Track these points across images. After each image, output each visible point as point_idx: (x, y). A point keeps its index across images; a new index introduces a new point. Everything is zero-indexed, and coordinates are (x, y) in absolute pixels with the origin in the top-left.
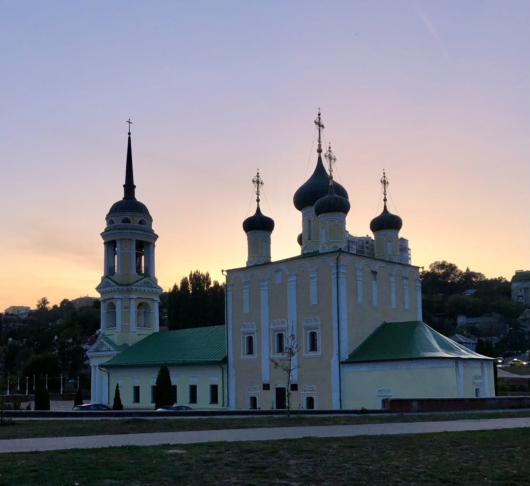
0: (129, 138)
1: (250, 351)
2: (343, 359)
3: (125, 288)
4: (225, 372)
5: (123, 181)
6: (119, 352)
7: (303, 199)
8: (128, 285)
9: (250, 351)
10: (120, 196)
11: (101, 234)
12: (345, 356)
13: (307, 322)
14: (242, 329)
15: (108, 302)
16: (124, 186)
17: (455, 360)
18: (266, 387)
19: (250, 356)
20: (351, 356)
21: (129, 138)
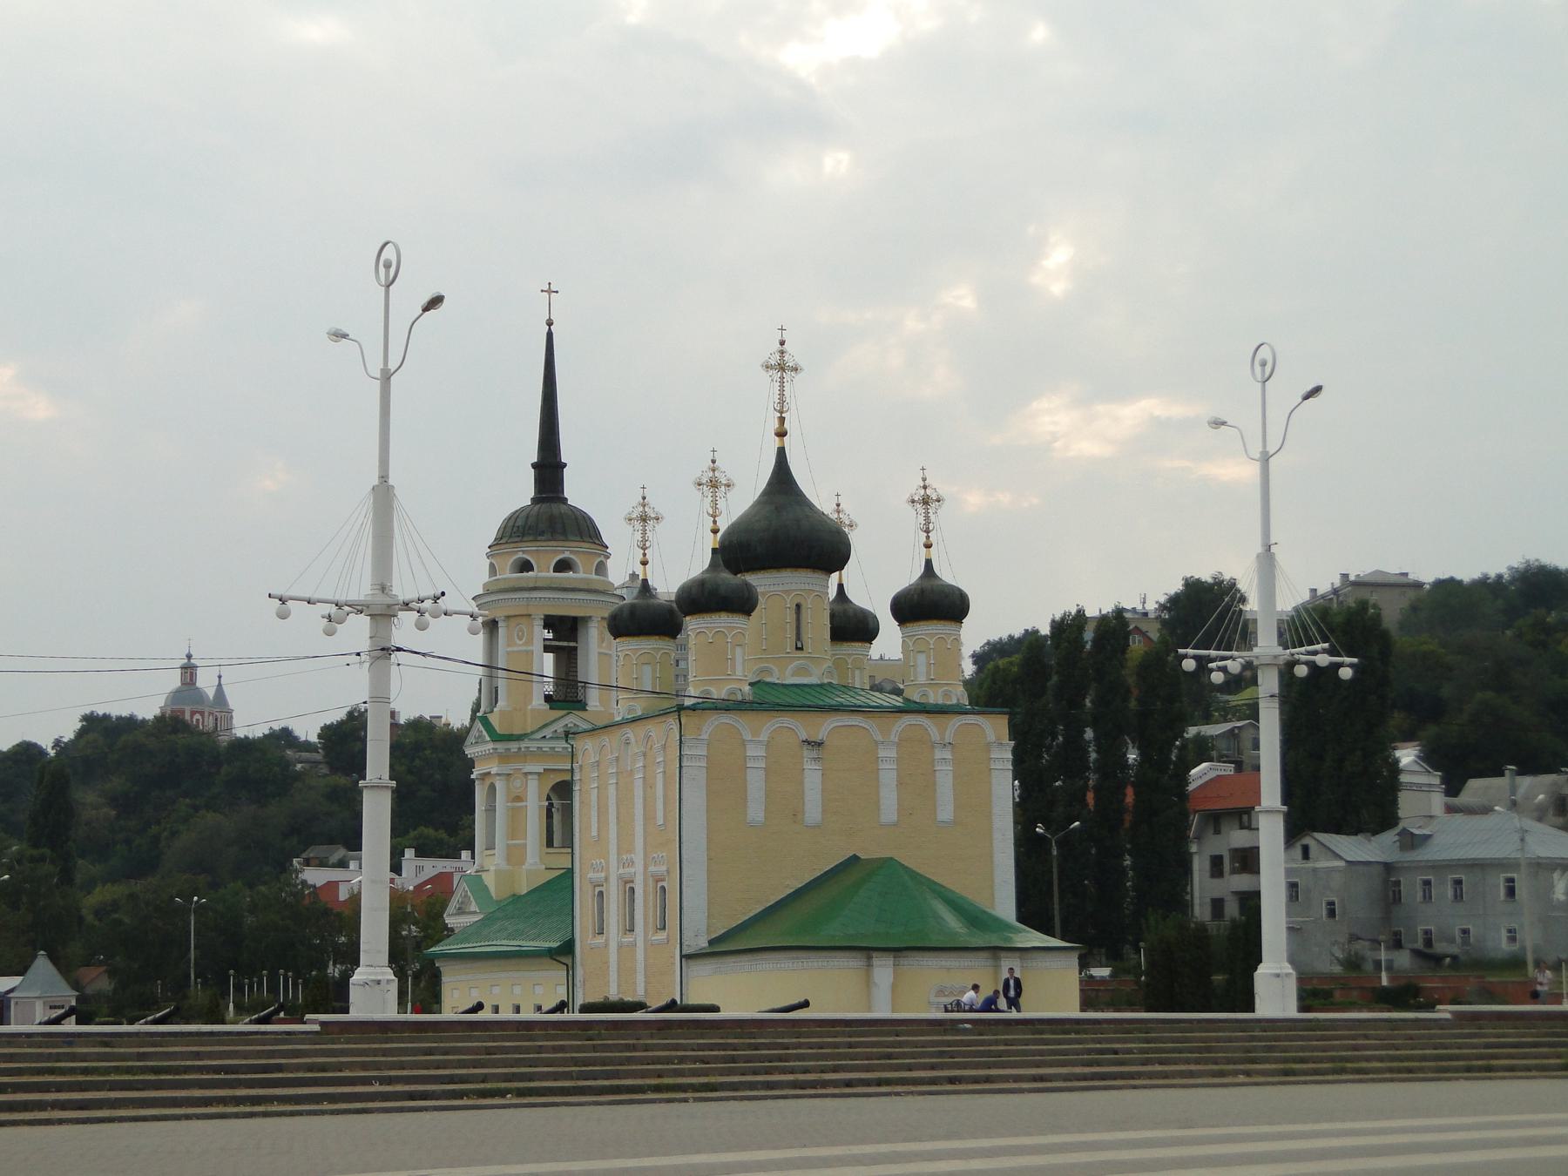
0: (550, 336)
3: (514, 746)
5: (530, 452)
8: (519, 738)
10: (522, 491)
15: (488, 782)
16: (534, 466)
21: (550, 336)
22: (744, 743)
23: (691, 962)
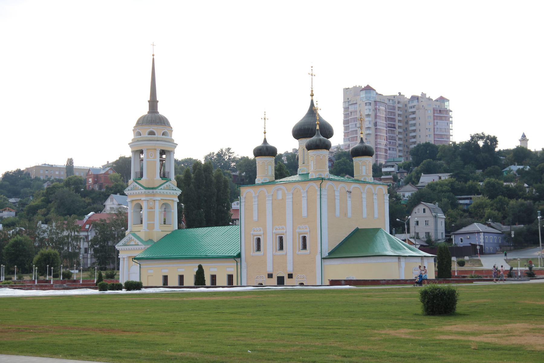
0: (153, 59)
1: (259, 249)
2: (323, 256)
3: (151, 191)
4: (239, 264)
6: (149, 246)
7: (300, 132)
8: (153, 188)
9: (259, 249)
10: (145, 110)
11: (346, 90)
12: (325, 254)
13: (300, 228)
14: (252, 232)
15: (135, 203)
16: (149, 101)
17: (397, 258)
18: (270, 276)
19: (258, 253)
20: (330, 254)
21: (153, 59)
22: (334, 191)
23: (325, 260)
